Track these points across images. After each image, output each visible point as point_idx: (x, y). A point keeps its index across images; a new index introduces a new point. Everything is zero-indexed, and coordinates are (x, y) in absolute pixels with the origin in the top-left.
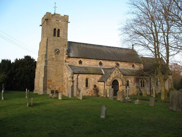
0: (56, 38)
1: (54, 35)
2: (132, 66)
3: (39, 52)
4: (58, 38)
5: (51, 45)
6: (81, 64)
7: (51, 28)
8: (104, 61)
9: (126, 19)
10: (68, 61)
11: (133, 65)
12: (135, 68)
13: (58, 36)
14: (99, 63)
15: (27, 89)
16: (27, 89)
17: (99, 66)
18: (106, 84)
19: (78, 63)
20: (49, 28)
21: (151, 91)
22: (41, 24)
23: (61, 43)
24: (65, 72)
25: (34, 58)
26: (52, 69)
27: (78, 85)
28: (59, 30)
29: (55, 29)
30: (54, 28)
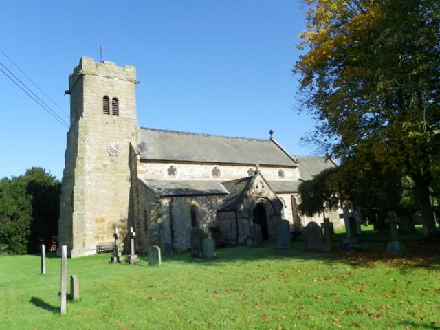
0: (110, 118)
1: (106, 111)
2: (278, 174)
3: (68, 155)
4: (115, 117)
5: (99, 134)
6: (174, 174)
7: (95, 94)
8: (221, 166)
9: (100, 67)
10: (143, 169)
11: (279, 173)
12: (285, 177)
13: (116, 113)
14: (213, 171)
15: (44, 247)
16: (44, 247)
17: (212, 178)
18: (239, 216)
19: (166, 173)
20: (91, 94)
21: (420, 104)
22: (68, 89)
23: (123, 130)
24: (138, 196)
25: (21, 174)
26: (103, 191)
27: (174, 223)
28: (115, 99)
29: (106, 98)
30: (103, 96)
